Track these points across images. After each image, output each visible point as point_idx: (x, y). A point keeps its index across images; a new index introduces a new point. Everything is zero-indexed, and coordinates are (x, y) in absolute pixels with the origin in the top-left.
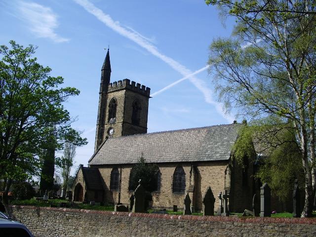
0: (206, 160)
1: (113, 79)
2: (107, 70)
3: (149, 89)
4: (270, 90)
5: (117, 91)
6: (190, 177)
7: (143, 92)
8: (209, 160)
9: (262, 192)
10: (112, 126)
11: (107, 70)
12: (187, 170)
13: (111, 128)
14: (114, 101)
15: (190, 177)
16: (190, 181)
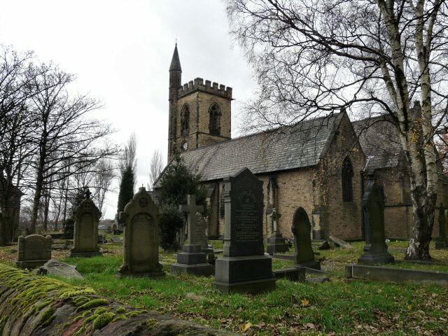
0: (287, 168)
1: (185, 79)
2: (175, 71)
3: (230, 89)
4: (442, 300)
5: (188, 94)
6: (268, 193)
7: (223, 93)
8: (291, 167)
9: (311, 233)
10: (186, 139)
11: (175, 71)
12: (266, 182)
13: (185, 142)
14: (186, 107)
15: (268, 193)
16: (269, 198)
